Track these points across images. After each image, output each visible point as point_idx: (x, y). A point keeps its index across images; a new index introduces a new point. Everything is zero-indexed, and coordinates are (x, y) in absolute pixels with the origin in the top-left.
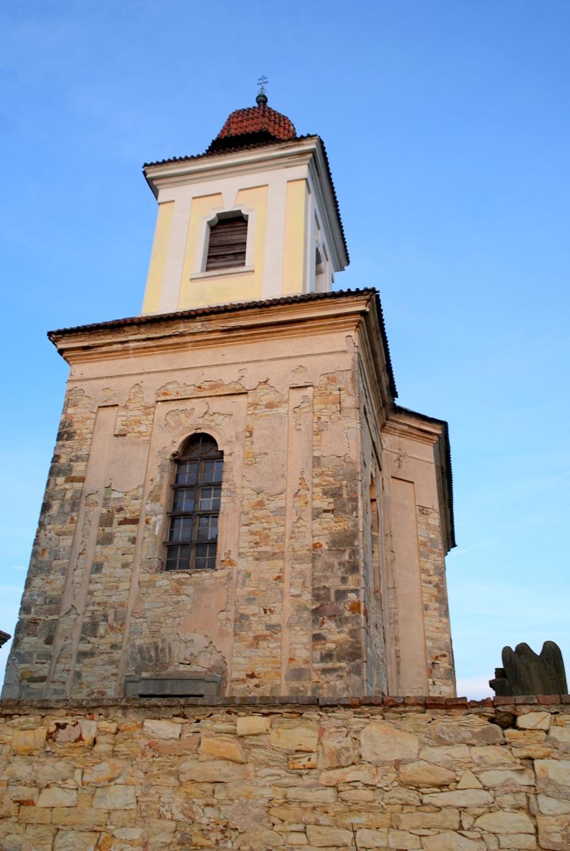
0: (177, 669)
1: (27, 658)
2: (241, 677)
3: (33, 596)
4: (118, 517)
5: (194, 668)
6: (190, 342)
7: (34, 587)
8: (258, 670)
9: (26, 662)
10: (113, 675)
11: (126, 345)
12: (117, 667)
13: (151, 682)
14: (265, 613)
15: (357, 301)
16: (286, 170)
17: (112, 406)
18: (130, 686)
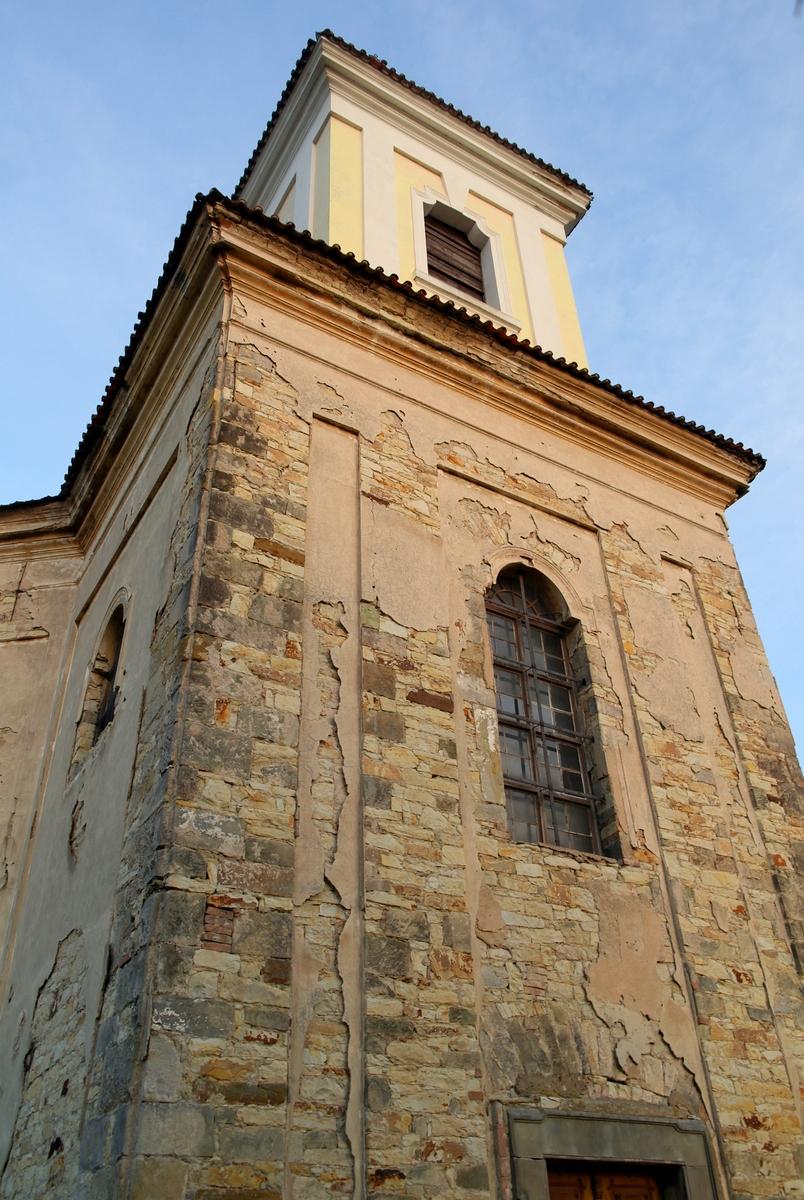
1: (215, 1019)
3: (210, 826)
6: (491, 388)
7: (209, 801)
8: (763, 1110)
9: (214, 1033)
11: (368, 322)
12: (478, 1076)
13: (569, 1124)
14: (740, 981)
15: (739, 467)
16: (533, 210)
17: (343, 428)
18: (520, 1129)
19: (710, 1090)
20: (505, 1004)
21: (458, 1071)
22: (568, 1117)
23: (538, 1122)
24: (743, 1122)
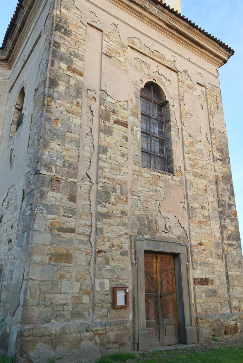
4: (113, 117)
6: (148, 18)
8: (203, 241)
9: (54, 214)
13: (151, 242)
14: (202, 208)
18: (138, 242)
19: (190, 235)
22: (151, 240)
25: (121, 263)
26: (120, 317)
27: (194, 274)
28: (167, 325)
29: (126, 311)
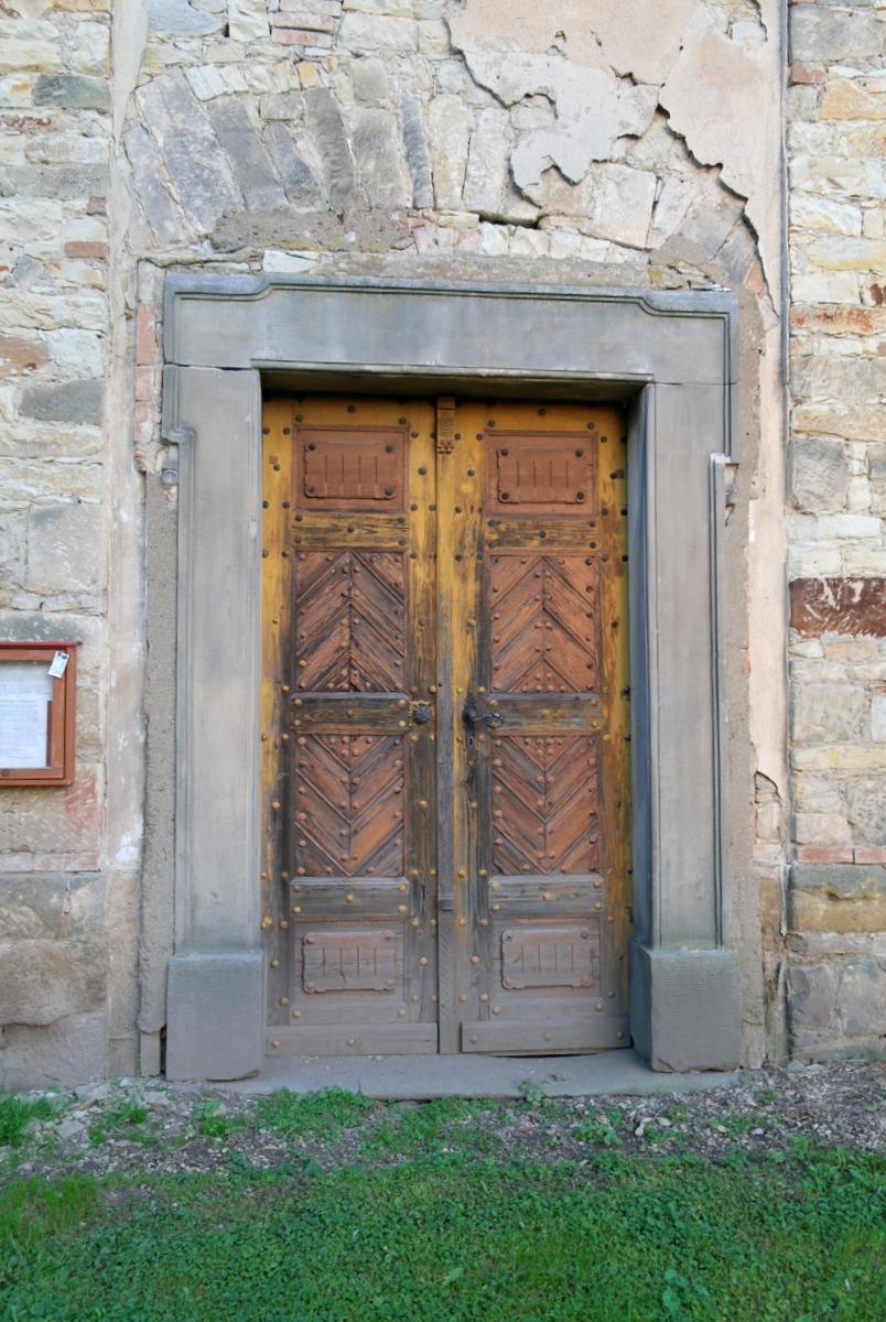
0: (466, 245)
2: (849, 301)
5: (564, 242)
10: (76, 250)
13: (333, 301)
18: (196, 315)
19: (786, 229)
20: (210, 70)
21: (47, 203)
22: (331, 287)
23: (247, 297)
24: (868, 296)
25: (26, 474)
26: (14, 851)
27: (794, 550)
28: (515, 915)
29: (68, 810)
